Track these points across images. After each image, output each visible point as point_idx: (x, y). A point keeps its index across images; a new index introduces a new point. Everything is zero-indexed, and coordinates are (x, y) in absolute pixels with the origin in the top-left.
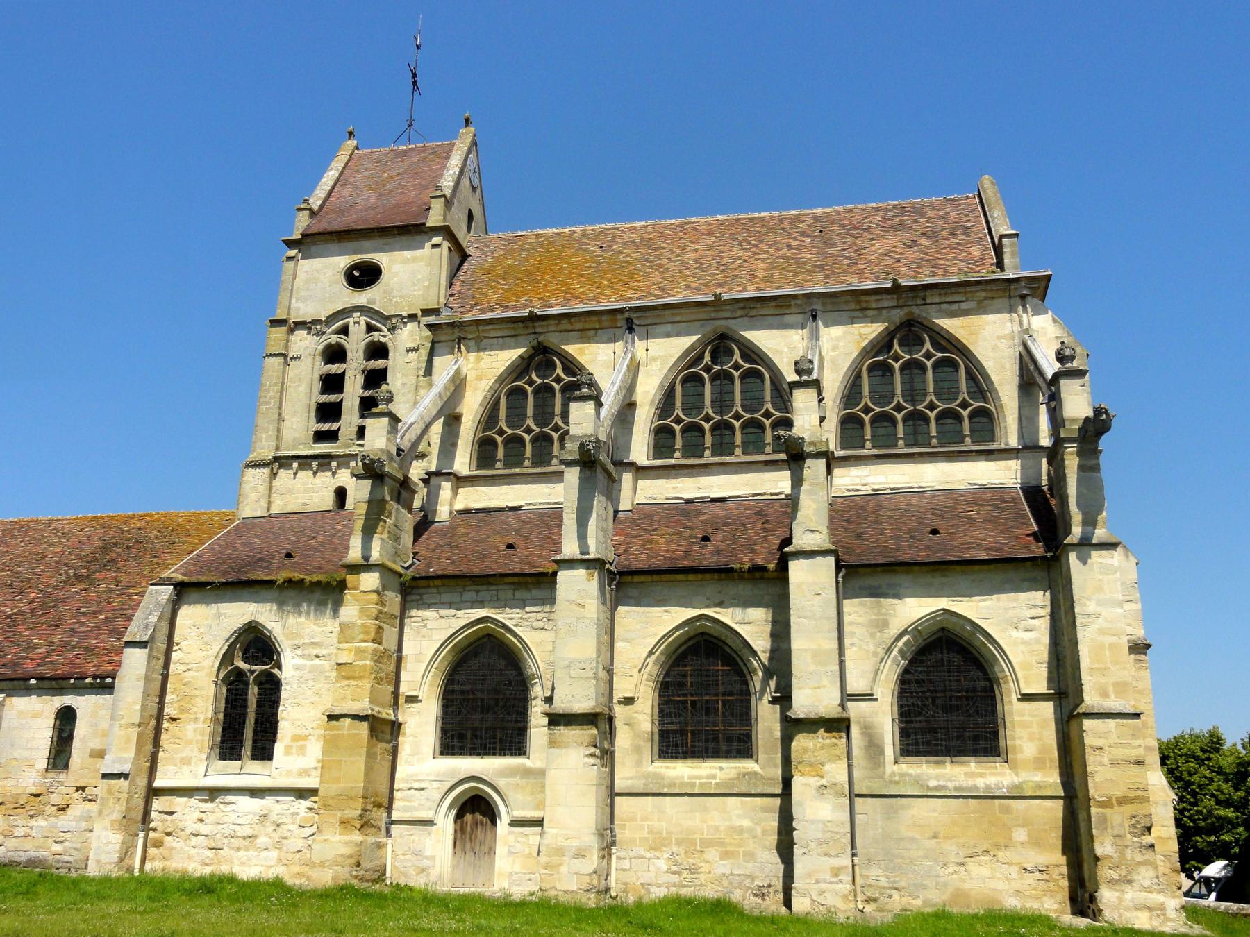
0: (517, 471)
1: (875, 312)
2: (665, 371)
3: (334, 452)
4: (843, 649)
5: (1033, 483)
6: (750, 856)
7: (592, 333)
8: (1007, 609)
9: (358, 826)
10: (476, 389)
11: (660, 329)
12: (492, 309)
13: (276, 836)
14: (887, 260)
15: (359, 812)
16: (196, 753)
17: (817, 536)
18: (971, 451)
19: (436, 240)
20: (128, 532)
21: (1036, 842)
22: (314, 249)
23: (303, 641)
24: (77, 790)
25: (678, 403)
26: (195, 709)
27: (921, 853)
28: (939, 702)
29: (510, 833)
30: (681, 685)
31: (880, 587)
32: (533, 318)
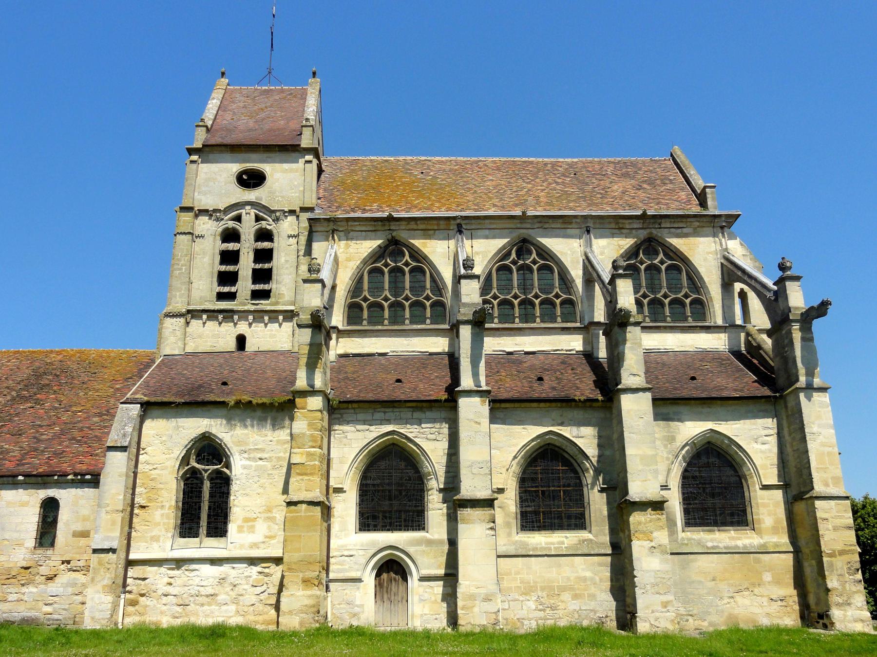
0: (380, 327)
1: (628, 231)
2: (485, 263)
3: (235, 308)
4: (654, 453)
5: (736, 349)
6: (592, 597)
7: (432, 232)
8: (750, 430)
9: (316, 583)
10: (346, 267)
11: (480, 232)
12: (353, 210)
13: (233, 594)
14: (624, 198)
15: (317, 573)
16: (164, 533)
17: (637, 378)
18: (520, 329)
19: (309, 157)
20: (51, 364)
21: (777, 582)
22: (211, 156)
23: (248, 448)
24: (63, 563)
25: (495, 285)
26: (160, 499)
27: (705, 591)
28: (708, 491)
29: (419, 586)
30: (533, 480)
31: (668, 414)
32: (390, 219)
